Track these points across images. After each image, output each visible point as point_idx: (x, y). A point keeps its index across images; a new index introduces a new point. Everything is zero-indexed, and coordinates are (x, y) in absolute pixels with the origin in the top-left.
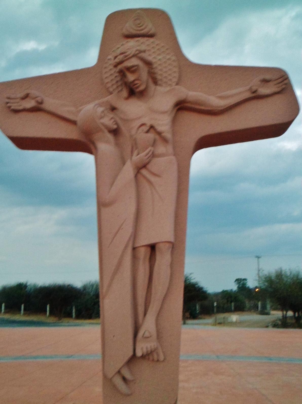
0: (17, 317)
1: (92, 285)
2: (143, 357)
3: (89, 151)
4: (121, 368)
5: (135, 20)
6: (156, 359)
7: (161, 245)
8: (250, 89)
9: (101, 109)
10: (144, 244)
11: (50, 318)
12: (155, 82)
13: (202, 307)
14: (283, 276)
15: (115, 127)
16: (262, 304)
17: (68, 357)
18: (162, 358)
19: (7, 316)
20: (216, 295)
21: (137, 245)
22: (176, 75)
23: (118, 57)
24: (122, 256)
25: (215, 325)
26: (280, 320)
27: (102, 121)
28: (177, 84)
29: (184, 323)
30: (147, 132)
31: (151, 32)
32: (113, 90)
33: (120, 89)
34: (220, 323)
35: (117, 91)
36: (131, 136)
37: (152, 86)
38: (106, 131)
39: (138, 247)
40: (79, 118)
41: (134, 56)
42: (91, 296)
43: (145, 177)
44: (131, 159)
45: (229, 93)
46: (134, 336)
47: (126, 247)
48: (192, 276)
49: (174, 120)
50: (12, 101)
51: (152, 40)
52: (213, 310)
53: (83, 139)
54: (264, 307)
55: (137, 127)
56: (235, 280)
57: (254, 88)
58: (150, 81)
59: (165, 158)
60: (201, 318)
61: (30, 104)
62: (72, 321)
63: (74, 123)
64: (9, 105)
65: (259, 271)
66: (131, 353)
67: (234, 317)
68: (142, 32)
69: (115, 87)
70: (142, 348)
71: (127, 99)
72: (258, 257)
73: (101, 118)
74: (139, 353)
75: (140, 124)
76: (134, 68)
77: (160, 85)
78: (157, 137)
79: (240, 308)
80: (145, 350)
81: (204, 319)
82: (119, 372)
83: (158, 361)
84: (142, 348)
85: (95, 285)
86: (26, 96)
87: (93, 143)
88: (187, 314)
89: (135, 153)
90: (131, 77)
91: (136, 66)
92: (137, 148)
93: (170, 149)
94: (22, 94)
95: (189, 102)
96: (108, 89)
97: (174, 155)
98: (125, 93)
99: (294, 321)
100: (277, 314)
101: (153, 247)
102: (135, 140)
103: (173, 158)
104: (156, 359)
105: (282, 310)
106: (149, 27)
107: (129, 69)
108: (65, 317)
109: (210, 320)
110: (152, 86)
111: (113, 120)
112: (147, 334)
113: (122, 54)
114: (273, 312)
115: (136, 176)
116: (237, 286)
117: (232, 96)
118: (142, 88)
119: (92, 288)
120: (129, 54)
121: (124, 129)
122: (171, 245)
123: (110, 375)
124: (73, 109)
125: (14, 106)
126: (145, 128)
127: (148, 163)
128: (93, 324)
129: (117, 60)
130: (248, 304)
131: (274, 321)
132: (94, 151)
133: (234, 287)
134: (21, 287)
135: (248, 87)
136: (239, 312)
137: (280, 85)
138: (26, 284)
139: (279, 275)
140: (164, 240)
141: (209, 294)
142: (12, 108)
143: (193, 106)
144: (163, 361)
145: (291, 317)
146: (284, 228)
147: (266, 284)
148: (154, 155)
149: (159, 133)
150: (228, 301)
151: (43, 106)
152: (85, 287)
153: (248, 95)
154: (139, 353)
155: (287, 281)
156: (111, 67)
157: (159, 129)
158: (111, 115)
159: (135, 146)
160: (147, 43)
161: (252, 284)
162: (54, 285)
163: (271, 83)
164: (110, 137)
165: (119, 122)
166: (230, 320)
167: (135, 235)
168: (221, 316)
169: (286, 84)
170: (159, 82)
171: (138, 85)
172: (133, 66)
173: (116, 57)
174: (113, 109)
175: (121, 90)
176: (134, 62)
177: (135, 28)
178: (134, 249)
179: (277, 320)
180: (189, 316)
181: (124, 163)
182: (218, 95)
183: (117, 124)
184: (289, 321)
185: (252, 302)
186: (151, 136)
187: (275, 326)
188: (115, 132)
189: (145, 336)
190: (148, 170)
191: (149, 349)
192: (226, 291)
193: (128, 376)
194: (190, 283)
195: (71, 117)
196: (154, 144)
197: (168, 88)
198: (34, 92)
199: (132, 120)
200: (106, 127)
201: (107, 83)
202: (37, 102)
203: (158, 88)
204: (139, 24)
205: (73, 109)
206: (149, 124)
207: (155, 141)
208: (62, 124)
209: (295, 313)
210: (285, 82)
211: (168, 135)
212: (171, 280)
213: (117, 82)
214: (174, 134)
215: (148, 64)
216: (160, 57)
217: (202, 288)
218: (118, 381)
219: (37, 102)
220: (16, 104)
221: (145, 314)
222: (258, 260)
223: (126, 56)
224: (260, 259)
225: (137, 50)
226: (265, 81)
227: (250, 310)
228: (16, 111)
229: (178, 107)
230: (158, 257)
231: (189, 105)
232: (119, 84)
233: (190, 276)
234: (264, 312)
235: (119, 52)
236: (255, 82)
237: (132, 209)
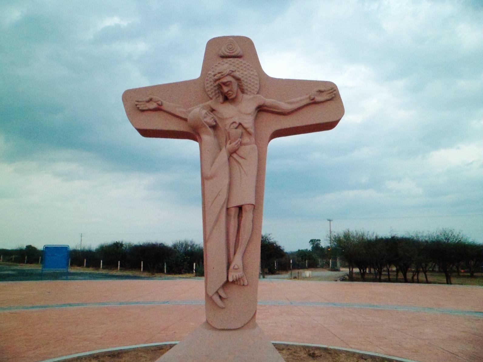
0: (114, 273)
1: (182, 244)
2: (233, 282)
3: (195, 139)
4: (218, 290)
5: (228, 45)
6: (242, 284)
7: (246, 207)
8: (310, 97)
9: (204, 112)
10: (234, 206)
11: (144, 273)
12: (243, 91)
13: (280, 264)
14: (350, 237)
15: (214, 124)
16: (332, 262)
17: (164, 303)
18: (246, 283)
19: (104, 272)
20: (292, 254)
21: (229, 207)
22: (258, 86)
23: (217, 75)
24: (220, 212)
25: (291, 279)
26: (347, 275)
27: (205, 120)
28: (258, 93)
29: (264, 277)
30: (237, 128)
31: (239, 55)
32: (213, 96)
33: (217, 96)
34: (295, 278)
35: (215, 97)
36: (226, 130)
37: (240, 95)
38: (208, 126)
39: (230, 208)
40: (190, 117)
41: (229, 75)
42: (181, 253)
43: (235, 159)
44: (226, 146)
45: (293, 100)
46: (228, 268)
47: (222, 207)
48: (271, 236)
49: (256, 118)
50: (139, 103)
51: (240, 60)
52: (290, 267)
53: (192, 132)
54: (335, 264)
55: (230, 124)
56: (310, 240)
57: (312, 97)
58: (239, 92)
59: (250, 146)
60: (278, 274)
61: (153, 106)
62: (163, 275)
63: (186, 120)
64: (138, 106)
65: (331, 232)
66: (225, 280)
67: (308, 273)
68: (233, 54)
69: (213, 94)
70: (233, 277)
71: (222, 103)
72: (330, 221)
73: (205, 117)
74: (231, 279)
75: (232, 122)
76: (228, 83)
77: (247, 93)
78: (244, 131)
79: (313, 265)
80: (235, 277)
81: (281, 274)
82: (217, 292)
83: (244, 285)
84: (233, 277)
85: (189, 242)
86: (151, 100)
87: (199, 135)
88: (266, 270)
89: (229, 142)
90: (226, 89)
91: (229, 82)
92: (230, 139)
93: (253, 139)
94: (147, 99)
95: (266, 106)
96: (208, 95)
97: (256, 144)
98: (221, 99)
99: (360, 277)
100: (345, 271)
101: (240, 208)
102: (229, 133)
103: (256, 146)
104: (242, 284)
105: (349, 267)
106: (238, 51)
107: (225, 84)
108: (157, 272)
109: (286, 275)
110: (240, 95)
111: (213, 119)
112: (236, 267)
113: (219, 73)
114: (342, 269)
115: (229, 159)
116: (312, 246)
117: (297, 102)
118: (234, 96)
119: (182, 246)
120: (225, 74)
121: (220, 125)
122: (253, 206)
123: (210, 294)
124: (184, 110)
125: (142, 107)
126: (235, 125)
127: (237, 150)
128: (181, 278)
129: (216, 77)
130: (320, 261)
131: (343, 277)
132: (198, 139)
133: (309, 247)
134: (117, 246)
135: (308, 96)
136: (313, 269)
137: (331, 94)
138: (122, 242)
139: (347, 236)
140: (248, 203)
141: (286, 253)
142: (140, 108)
143: (270, 109)
144: (247, 285)
145: (356, 273)
146: (352, 194)
147: (336, 243)
148: (241, 144)
149: (245, 129)
150: (302, 259)
151: (162, 107)
152: (175, 246)
153: (308, 101)
154: (231, 279)
155: (353, 241)
156: (212, 83)
157: (246, 126)
158: (212, 115)
159: (228, 137)
160: (237, 62)
161: (324, 244)
162: (148, 244)
163: (324, 93)
164: (211, 131)
165: (218, 121)
166: (303, 275)
167: (228, 200)
168: (295, 272)
169: (335, 94)
170: (246, 91)
171: (231, 94)
172: (227, 82)
173: (215, 75)
174: (213, 110)
175: (219, 96)
176: (229, 79)
177: (229, 51)
178: (228, 209)
179: (345, 275)
180: (268, 272)
181: (221, 150)
182: (287, 101)
183: (216, 122)
184: (354, 275)
185: (324, 260)
186: (240, 130)
187: (343, 279)
188: (215, 127)
189: (235, 268)
190: (236, 153)
191: (238, 277)
192: (302, 251)
193: (223, 295)
194: (269, 243)
195: (183, 116)
196: (242, 136)
197: (252, 96)
198: (156, 97)
199: (227, 119)
200: (208, 124)
201: (208, 91)
202: (158, 104)
203: (245, 96)
204: (230, 48)
205: (184, 110)
206: (238, 122)
207: (242, 134)
208: (175, 120)
209: (360, 270)
210: (335, 92)
211: (252, 130)
212: (252, 231)
213: (215, 90)
214: (256, 129)
215: (238, 79)
216: (246, 73)
217: (280, 247)
218: (216, 298)
219: (158, 104)
220: (142, 106)
221: (235, 253)
222: (330, 222)
223: (222, 75)
224: (331, 222)
225: (230, 71)
226: (321, 92)
227: (322, 267)
228: (143, 111)
229: (259, 109)
230: (244, 214)
231: (265, 108)
232: (217, 92)
233: (269, 236)
234: (334, 269)
235: (217, 71)
236: (313, 92)
237: (227, 181)
